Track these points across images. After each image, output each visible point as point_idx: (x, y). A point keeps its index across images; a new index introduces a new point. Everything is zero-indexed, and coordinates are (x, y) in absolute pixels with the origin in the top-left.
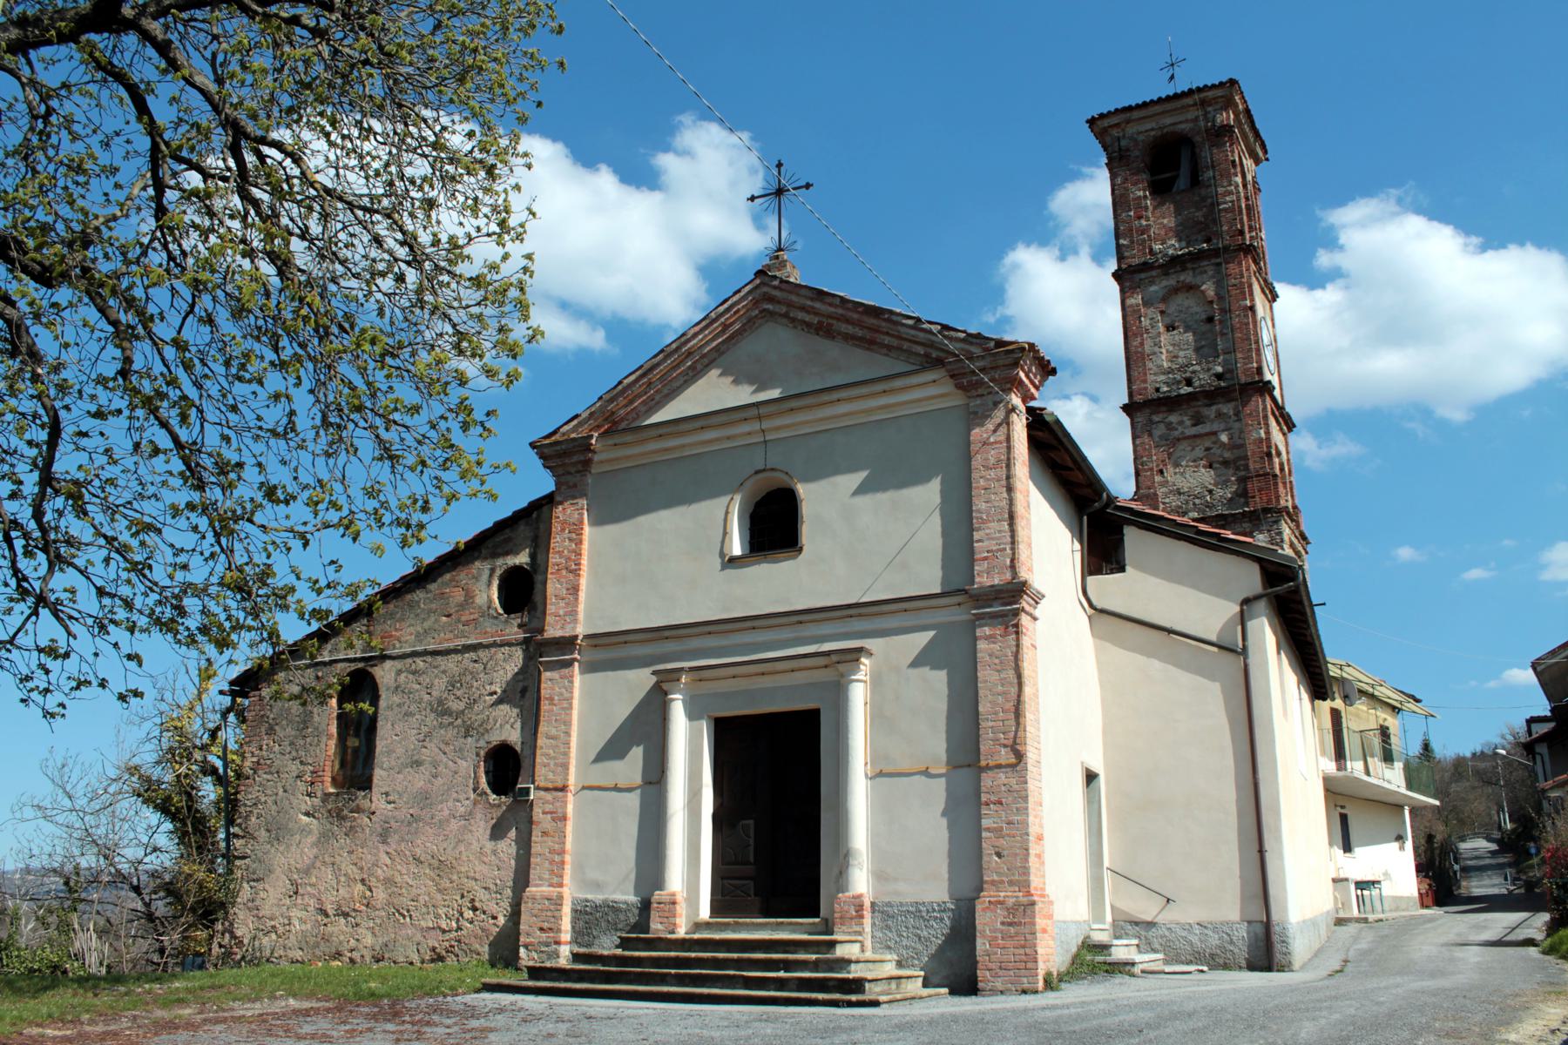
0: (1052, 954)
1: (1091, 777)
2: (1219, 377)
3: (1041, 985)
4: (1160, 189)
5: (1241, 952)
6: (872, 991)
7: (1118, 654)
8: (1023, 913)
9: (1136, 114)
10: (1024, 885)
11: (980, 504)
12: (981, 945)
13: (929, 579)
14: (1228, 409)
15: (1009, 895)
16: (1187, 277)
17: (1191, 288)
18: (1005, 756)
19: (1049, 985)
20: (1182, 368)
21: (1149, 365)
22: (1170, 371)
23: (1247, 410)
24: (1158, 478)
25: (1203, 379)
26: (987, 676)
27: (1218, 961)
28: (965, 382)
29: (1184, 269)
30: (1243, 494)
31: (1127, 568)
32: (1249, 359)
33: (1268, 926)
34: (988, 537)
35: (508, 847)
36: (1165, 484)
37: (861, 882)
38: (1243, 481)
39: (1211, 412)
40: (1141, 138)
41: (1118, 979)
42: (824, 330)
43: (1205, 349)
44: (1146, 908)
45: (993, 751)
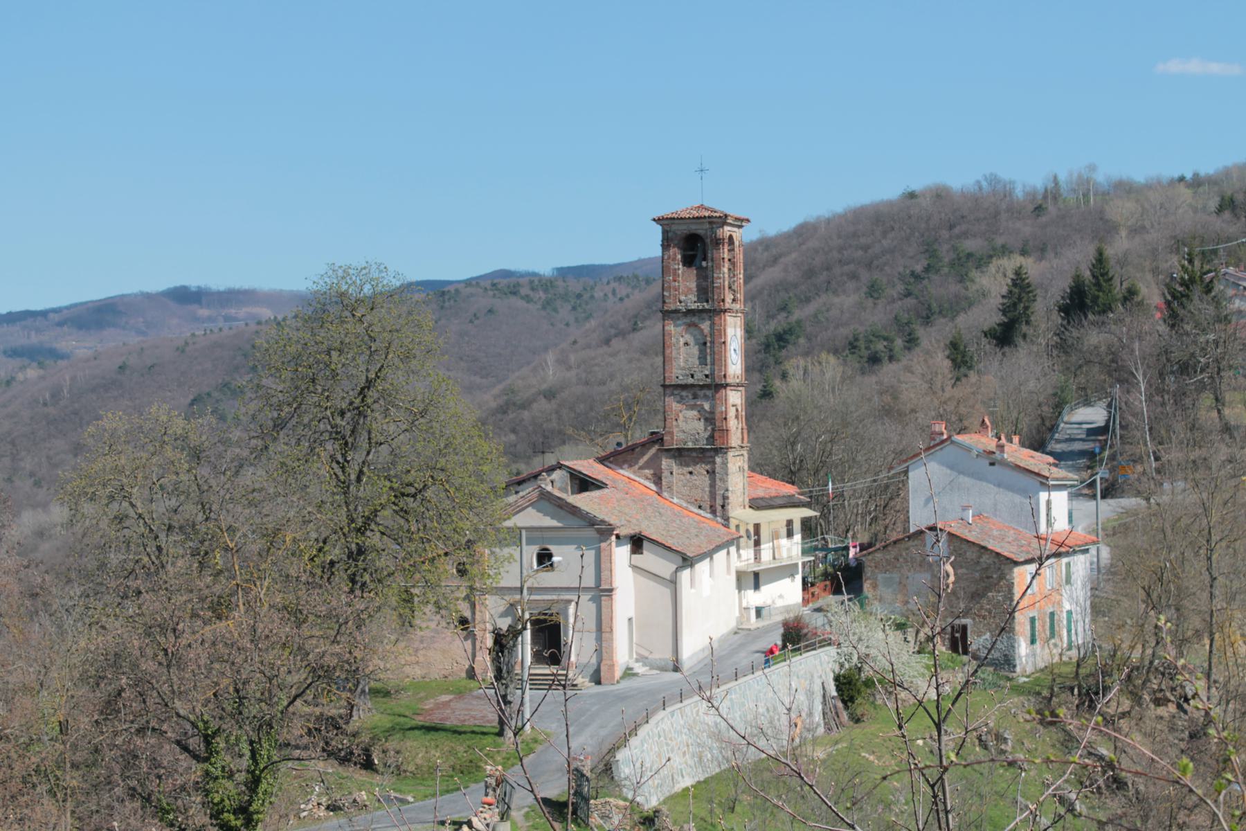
0: (618, 673)
1: (630, 619)
2: (707, 376)
3: (524, 533)
4: (688, 261)
5: (671, 667)
6: (579, 687)
7: (638, 576)
8: (612, 667)
9: (676, 221)
10: (612, 660)
11: (603, 566)
12: (602, 674)
13: (592, 584)
14: (709, 393)
15: (609, 662)
16: (695, 319)
17: (695, 325)
18: (608, 630)
19: (618, 682)
20: (689, 369)
21: (674, 364)
22: (683, 369)
23: (717, 396)
24: (674, 423)
25: (699, 378)
26: (604, 610)
27: (663, 669)
28: (600, 532)
29: (694, 315)
30: (712, 437)
31: (645, 552)
32: (720, 370)
33: (677, 660)
34: (604, 575)
35: (469, 643)
36: (678, 426)
37: (573, 658)
38: (713, 430)
39: (701, 393)
40: (679, 233)
41: (635, 678)
42: (560, 507)
43: (702, 360)
44: (646, 654)
45: (605, 627)
